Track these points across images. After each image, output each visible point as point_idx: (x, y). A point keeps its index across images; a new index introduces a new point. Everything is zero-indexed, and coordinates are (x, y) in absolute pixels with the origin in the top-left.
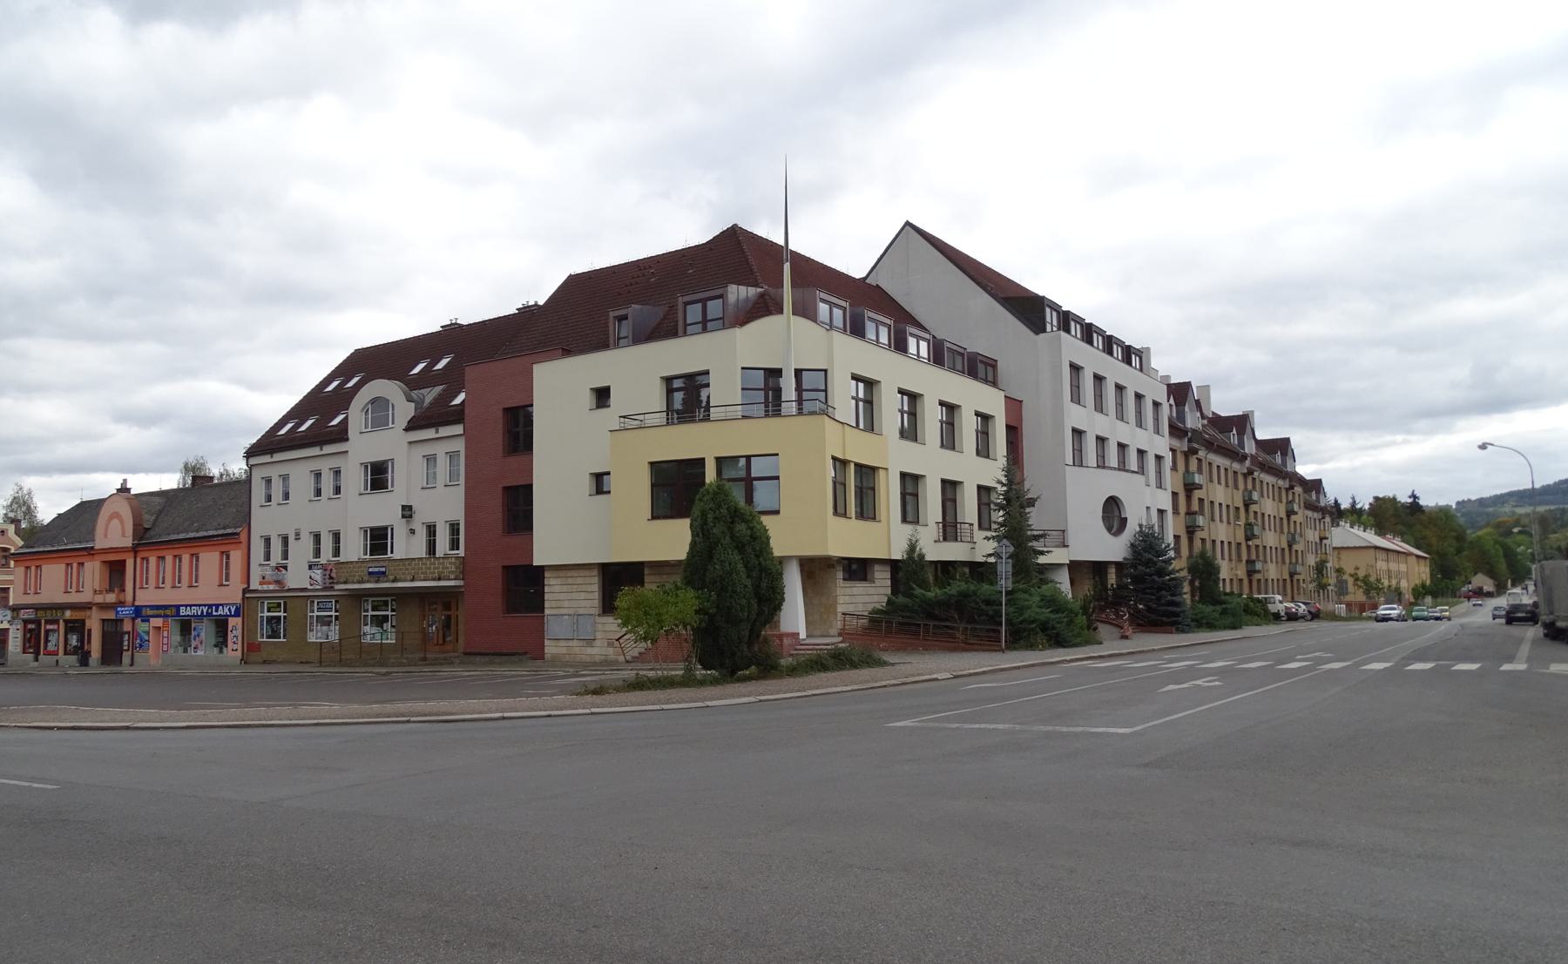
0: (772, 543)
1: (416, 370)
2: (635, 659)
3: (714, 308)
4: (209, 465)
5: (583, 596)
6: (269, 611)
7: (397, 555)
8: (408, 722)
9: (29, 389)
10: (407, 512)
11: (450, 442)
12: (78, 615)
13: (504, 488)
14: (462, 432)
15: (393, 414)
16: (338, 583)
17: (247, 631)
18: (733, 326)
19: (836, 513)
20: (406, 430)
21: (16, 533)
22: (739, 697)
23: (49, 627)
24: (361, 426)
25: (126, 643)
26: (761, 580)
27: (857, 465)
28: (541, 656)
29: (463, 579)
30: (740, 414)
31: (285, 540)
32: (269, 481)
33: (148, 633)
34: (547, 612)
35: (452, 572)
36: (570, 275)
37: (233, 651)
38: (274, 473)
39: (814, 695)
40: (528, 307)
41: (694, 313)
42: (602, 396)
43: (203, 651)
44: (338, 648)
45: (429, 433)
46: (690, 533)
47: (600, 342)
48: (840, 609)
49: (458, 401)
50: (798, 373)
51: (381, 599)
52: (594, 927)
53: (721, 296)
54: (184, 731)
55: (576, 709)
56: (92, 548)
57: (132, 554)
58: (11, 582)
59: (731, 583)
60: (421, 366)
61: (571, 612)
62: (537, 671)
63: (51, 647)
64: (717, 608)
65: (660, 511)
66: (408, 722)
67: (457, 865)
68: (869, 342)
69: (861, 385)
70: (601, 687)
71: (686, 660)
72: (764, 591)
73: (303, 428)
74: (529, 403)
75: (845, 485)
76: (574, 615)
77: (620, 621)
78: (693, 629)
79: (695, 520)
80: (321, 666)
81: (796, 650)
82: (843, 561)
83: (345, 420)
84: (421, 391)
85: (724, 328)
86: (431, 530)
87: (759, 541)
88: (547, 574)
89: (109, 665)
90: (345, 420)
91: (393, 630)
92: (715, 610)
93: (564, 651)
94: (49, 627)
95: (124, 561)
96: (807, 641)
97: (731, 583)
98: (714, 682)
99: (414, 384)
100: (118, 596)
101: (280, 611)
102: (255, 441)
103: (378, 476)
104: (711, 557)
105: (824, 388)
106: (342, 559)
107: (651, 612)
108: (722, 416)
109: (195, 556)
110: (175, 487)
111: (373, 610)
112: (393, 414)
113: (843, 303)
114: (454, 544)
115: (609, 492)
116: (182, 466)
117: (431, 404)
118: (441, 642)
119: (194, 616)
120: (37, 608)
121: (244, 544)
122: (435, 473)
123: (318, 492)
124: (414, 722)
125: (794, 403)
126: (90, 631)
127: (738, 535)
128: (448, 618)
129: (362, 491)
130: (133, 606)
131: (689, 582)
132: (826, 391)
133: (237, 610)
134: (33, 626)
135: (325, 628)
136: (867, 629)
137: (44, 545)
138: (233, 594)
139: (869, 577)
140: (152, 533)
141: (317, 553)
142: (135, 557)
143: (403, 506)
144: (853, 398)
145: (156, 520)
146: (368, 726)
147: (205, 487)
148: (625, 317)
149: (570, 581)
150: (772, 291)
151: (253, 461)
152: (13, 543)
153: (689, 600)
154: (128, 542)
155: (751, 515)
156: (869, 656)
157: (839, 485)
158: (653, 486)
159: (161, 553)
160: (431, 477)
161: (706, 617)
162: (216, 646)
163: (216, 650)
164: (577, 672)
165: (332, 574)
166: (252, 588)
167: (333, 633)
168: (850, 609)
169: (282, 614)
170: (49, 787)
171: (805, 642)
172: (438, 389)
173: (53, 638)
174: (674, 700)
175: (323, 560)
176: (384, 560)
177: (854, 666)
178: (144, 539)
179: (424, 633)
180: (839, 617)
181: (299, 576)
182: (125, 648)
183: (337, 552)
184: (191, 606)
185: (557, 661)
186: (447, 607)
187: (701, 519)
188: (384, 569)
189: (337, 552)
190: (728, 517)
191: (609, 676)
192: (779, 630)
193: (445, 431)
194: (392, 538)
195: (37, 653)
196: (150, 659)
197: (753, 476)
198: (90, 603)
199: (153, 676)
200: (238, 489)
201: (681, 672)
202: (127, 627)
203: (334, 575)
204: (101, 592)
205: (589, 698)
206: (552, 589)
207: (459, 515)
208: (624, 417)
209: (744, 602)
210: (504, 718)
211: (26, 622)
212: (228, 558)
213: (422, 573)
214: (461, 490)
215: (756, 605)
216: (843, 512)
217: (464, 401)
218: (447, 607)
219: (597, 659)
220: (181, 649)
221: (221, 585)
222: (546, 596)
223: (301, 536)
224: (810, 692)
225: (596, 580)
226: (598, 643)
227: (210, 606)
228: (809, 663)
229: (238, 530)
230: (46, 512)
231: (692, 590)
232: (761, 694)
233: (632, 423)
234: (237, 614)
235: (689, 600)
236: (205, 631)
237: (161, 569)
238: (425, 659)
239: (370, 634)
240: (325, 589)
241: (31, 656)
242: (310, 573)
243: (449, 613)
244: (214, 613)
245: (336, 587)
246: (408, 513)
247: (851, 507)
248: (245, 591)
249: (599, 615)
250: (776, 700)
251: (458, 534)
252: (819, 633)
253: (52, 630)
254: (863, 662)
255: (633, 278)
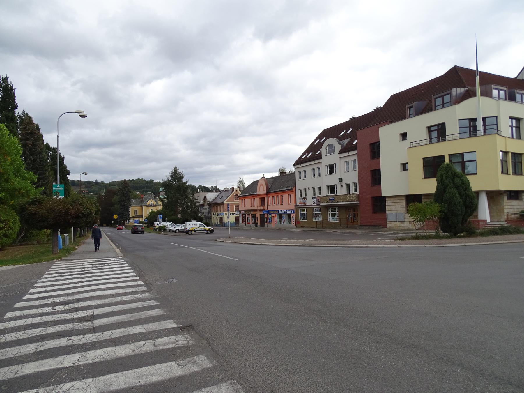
0: (471, 185)
1: (342, 134)
2: (419, 229)
3: (447, 98)
4: (286, 169)
5: (399, 206)
6: (302, 212)
7: (338, 194)
8: (336, 247)
9: (244, 151)
10: (340, 180)
11: (353, 156)
12: (254, 213)
13: (371, 170)
14: (356, 153)
15: (335, 149)
16: (321, 203)
17: (297, 218)
18: (455, 104)
19: (502, 172)
20: (339, 154)
21: (239, 191)
22: (457, 243)
23: (248, 216)
24: (325, 153)
25: (266, 221)
26: (466, 199)
27: (512, 153)
28: (386, 227)
29: (359, 201)
30: (458, 137)
31: (305, 190)
32: (300, 173)
33: (271, 218)
34: (387, 212)
35: (355, 199)
36: (392, 95)
37: (293, 224)
38: (301, 170)
39: (490, 244)
40: (378, 108)
41: (439, 101)
42: (404, 136)
43: (285, 224)
44: (322, 223)
45: (346, 154)
46: (436, 183)
47: (403, 117)
48: (506, 211)
49: (355, 143)
50: (484, 119)
51: (334, 208)
52: (374, 322)
53: (450, 94)
54: (274, 246)
55: (393, 245)
56: (257, 194)
57: (266, 195)
58: (239, 204)
59: (453, 201)
60: (343, 133)
61: (396, 212)
62: (384, 232)
63: (249, 222)
64: (448, 210)
65: (427, 176)
66: (336, 247)
67: (335, 295)
68: (518, 102)
69: (514, 121)
70: (403, 238)
71: (436, 229)
72: (468, 204)
73: (309, 156)
74: (378, 141)
75: (507, 162)
76: (397, 213)
77: (409, 215)
78: (438, 218)
79: (439, 178)
80: (317, 228)
81: (485, 226)
82: (507, 192)
83: (321, 152)
84: (343, 141)
85: (451, 105)
86: (348, 185)
87: (467, 185)
88: (387, 199)
89: (262, 227)
90: (321, 152)
91: (338, 218)
92: (447, 211)
93: (394, 225)
94: (248, 216)
95: (264, 198)
96: (491, 223)
97: (453, 201)
98: (448, 237)
99: (340, 139)
100: (263, 208)
101: (336, 211)
102: (296, 161)
103: (331, 169)
104: (445, 191)
105: (496, 124)
106: (322, 196)
107: (421, 212)
108: (451, 139)
109: (282, 196)
110: (278, 176)
111: (331, 211)
112: (335, 149)
113: (505, 89)
114: (356, 190)
115: (407, 170)
116: (279, 170)
117: (347, 145)
118: (353, 222)
119: (282, 213)
120: (245, 211)
121: (294, 192)
122: (348, 167)
123: (314, 175)
124: (338, 247)
125: (482, 131)
126: (257, 217)
127: (456, 183)
128: (355, 214)
129: (327, 174)
130: (267, 210)
131: (436, 201)
132: (497, 125)
133: (293, 211)
134: (244, 216)
135: (318, 217)
136: (519, 219)
137: (245, 194)
138: (292, 207)
139: (520, 198)
140: (270, 189)
141: (315, 194)
142: (267, 197)
143: (339, 178)
144: (510, 126)
145: (272, 186)
146: (324, 247)
147: (284, 175)
148: (412, 107)
149: (395, 201)
150: (472, 88)
151: (296, 167)
152: (239, 193)
153: (436, 207)
154: (265, 192)
155: (461, 175)
156: (518, 230)
157: (504, 162)
158: (424, 166)
159: (273, 195)
160: (347, 168)
161: (444, 213)
162: (288, 222)
163: (289, 223)
164: (398, 232)
165: (319, 200)
166: (297, 205)
167: (320, 219)
168: (511, 211)
169: (306, 213)
170: (236, 259)
171: (489, 224)
172: (349, 139)
173: (249, 219)
174: (430, 244)
175: (316, 196)
176: (334, 196)
177: (511, 233)
178: (269, 191)
179: (347, 218)
180: (505, 214)
181: (310, 201)
182: (266, 222)
183: (320, 194)
184: (281, 210)
185: (391, 229)
186: (354, 210)
187: (440, 177)
188: (334, 199)
189: (320, 194)
190: (452, 176)
191: (409, 234)
192: (478, 219)
193: (351, 153)
194: (336, 189)
195: (245, 223)
196: (272, 225)
197: (465, 160)
198: (257, 209)
199: (272, 230)
200: (293, 175)
201: (434, 234)
202: (266, 216)
203: (319, 201)
204: (259, 206)
205: (398, 241)
206: (389, 204)
207: (356, 180)
208: (412, 143)
209: (459, 208)
210: (367, 247)
211: (243, 215)
212: (290, 196)
213: (346, 200)
214: (357, 172)
215: (464, 209)
216: (506, 172)
217: (356, 143)
218: (354, 210)
219: (406, 228)
220: (280, 223)
221: (289, 204)
222: (387, 207)
223: (310, 189)
224: (489, 243)
225: (404, 201)
226: (406, 223)
227: (286, 210)
228: (489, 231)
229: (292, 188)
230: (247, 184)
231: (437, 204)
232: (467, 243)
233: (416, 145)
234: (293, 213)
235: (436, 207)
236: (285, 217)
237: (273, 199)
238: (347, 227)
239: (331, 219)
240: (317, 205)
241: (244, 224)
242: (313, 200)
243: (355, 212)
244: (288, 212)
245: (321, 204)
246: (340, 180)
247: (510, 170)
248: (296, 206)
249: (406, 213)
250: (473, 245)
251: (357, 187)
252: (496, 220)
253: (249, 217)
254: (515, 232)
255: (415, 92)
